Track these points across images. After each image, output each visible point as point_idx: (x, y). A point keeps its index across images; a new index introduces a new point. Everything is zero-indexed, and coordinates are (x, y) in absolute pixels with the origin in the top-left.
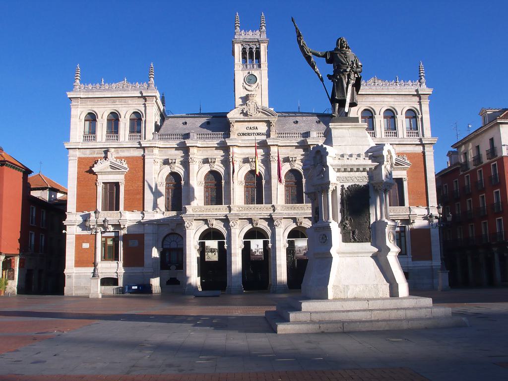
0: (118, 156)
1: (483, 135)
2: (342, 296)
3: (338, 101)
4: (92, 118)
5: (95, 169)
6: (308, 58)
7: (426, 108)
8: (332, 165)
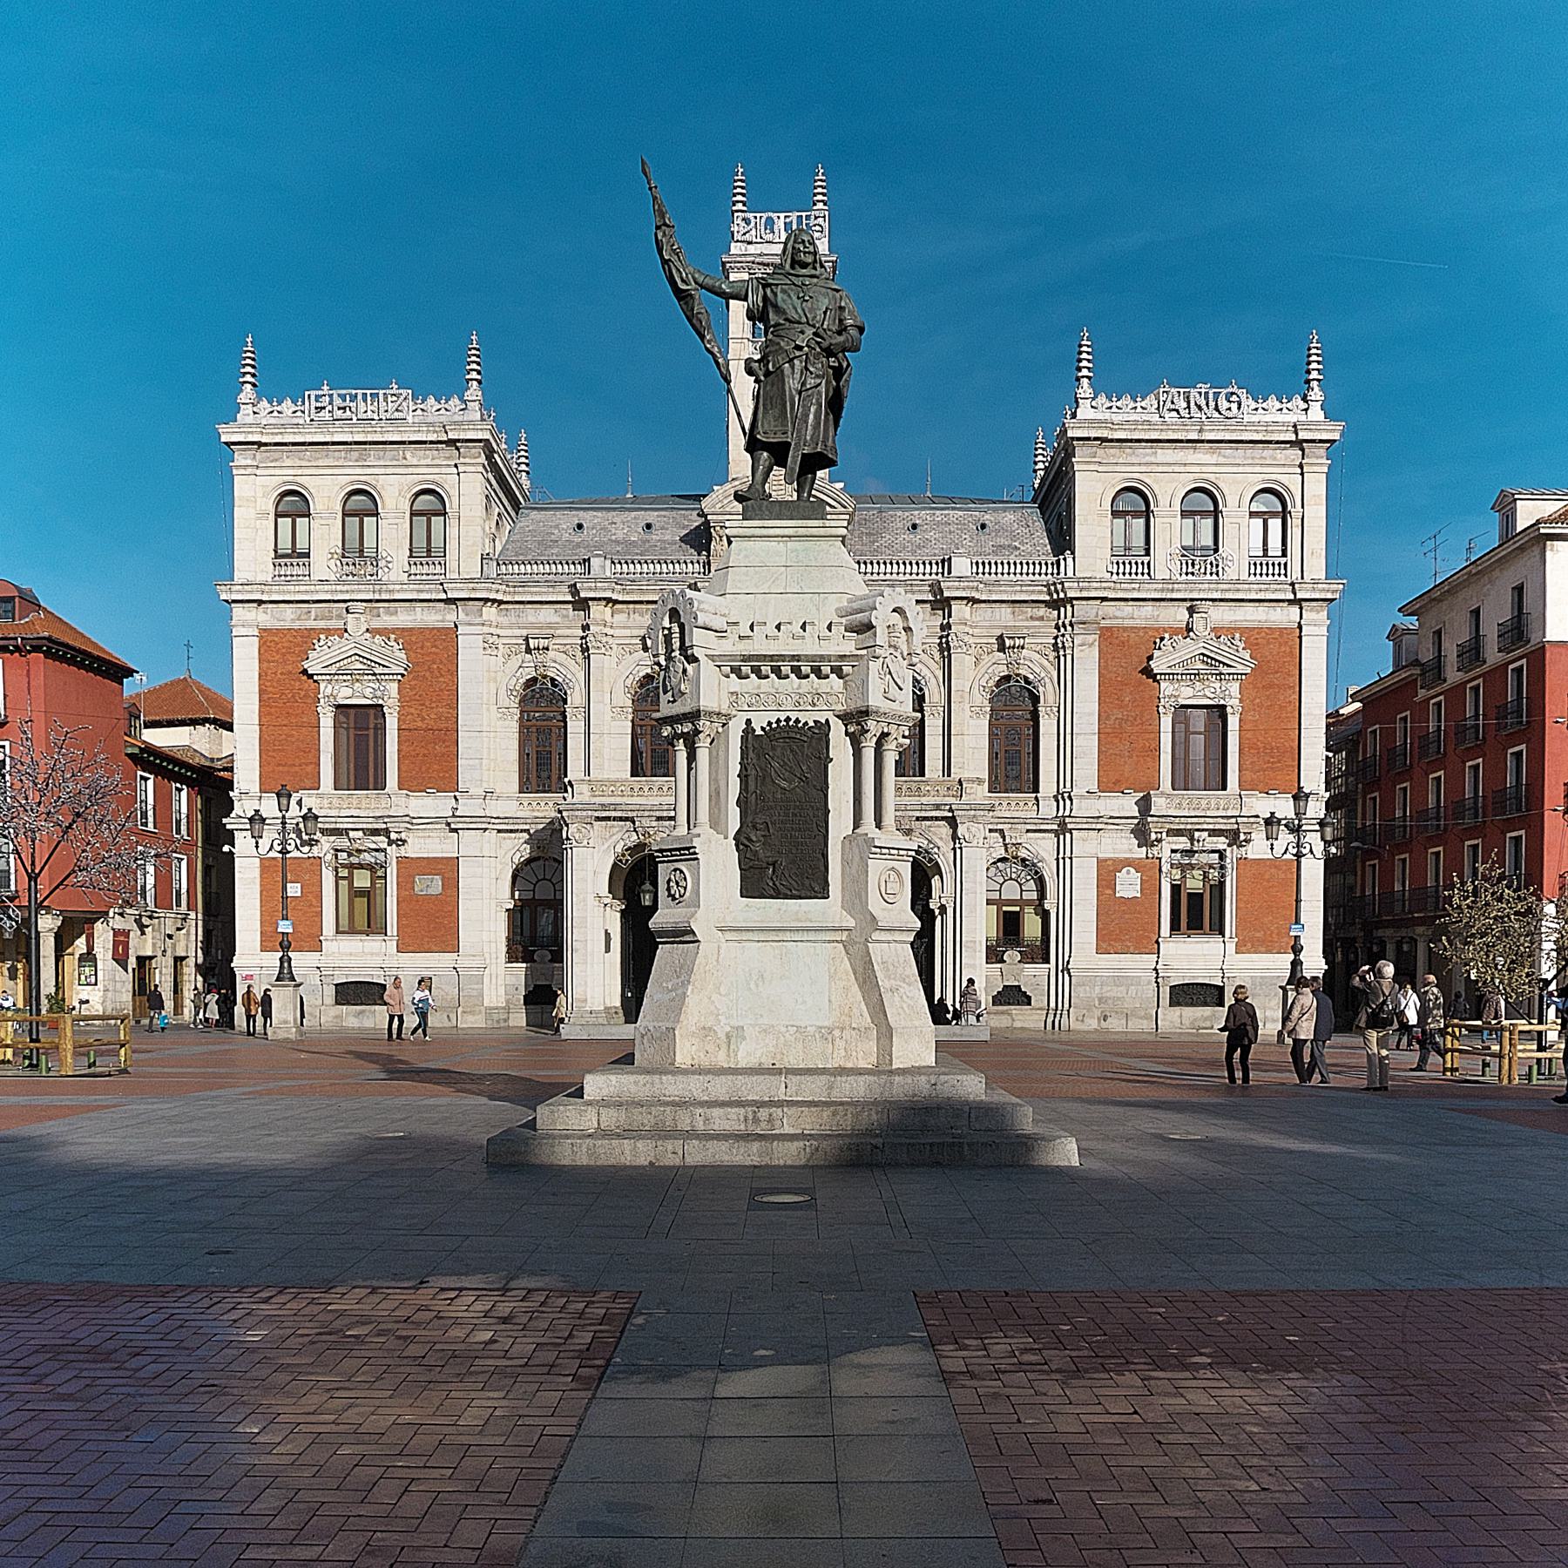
0: (376, 624)
1: (1497, 573)
2: (722, 1060)
3: (767, 447)
4: (293, 504)
5: (1157, 666)
6: (681, 296)
7: (1317, 485)
8: (711, 657)
